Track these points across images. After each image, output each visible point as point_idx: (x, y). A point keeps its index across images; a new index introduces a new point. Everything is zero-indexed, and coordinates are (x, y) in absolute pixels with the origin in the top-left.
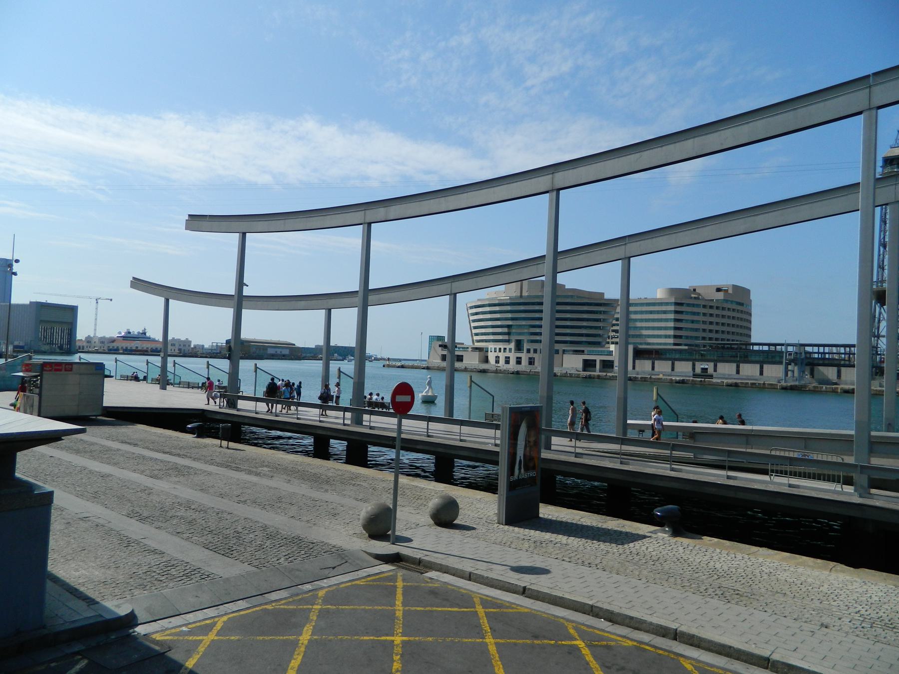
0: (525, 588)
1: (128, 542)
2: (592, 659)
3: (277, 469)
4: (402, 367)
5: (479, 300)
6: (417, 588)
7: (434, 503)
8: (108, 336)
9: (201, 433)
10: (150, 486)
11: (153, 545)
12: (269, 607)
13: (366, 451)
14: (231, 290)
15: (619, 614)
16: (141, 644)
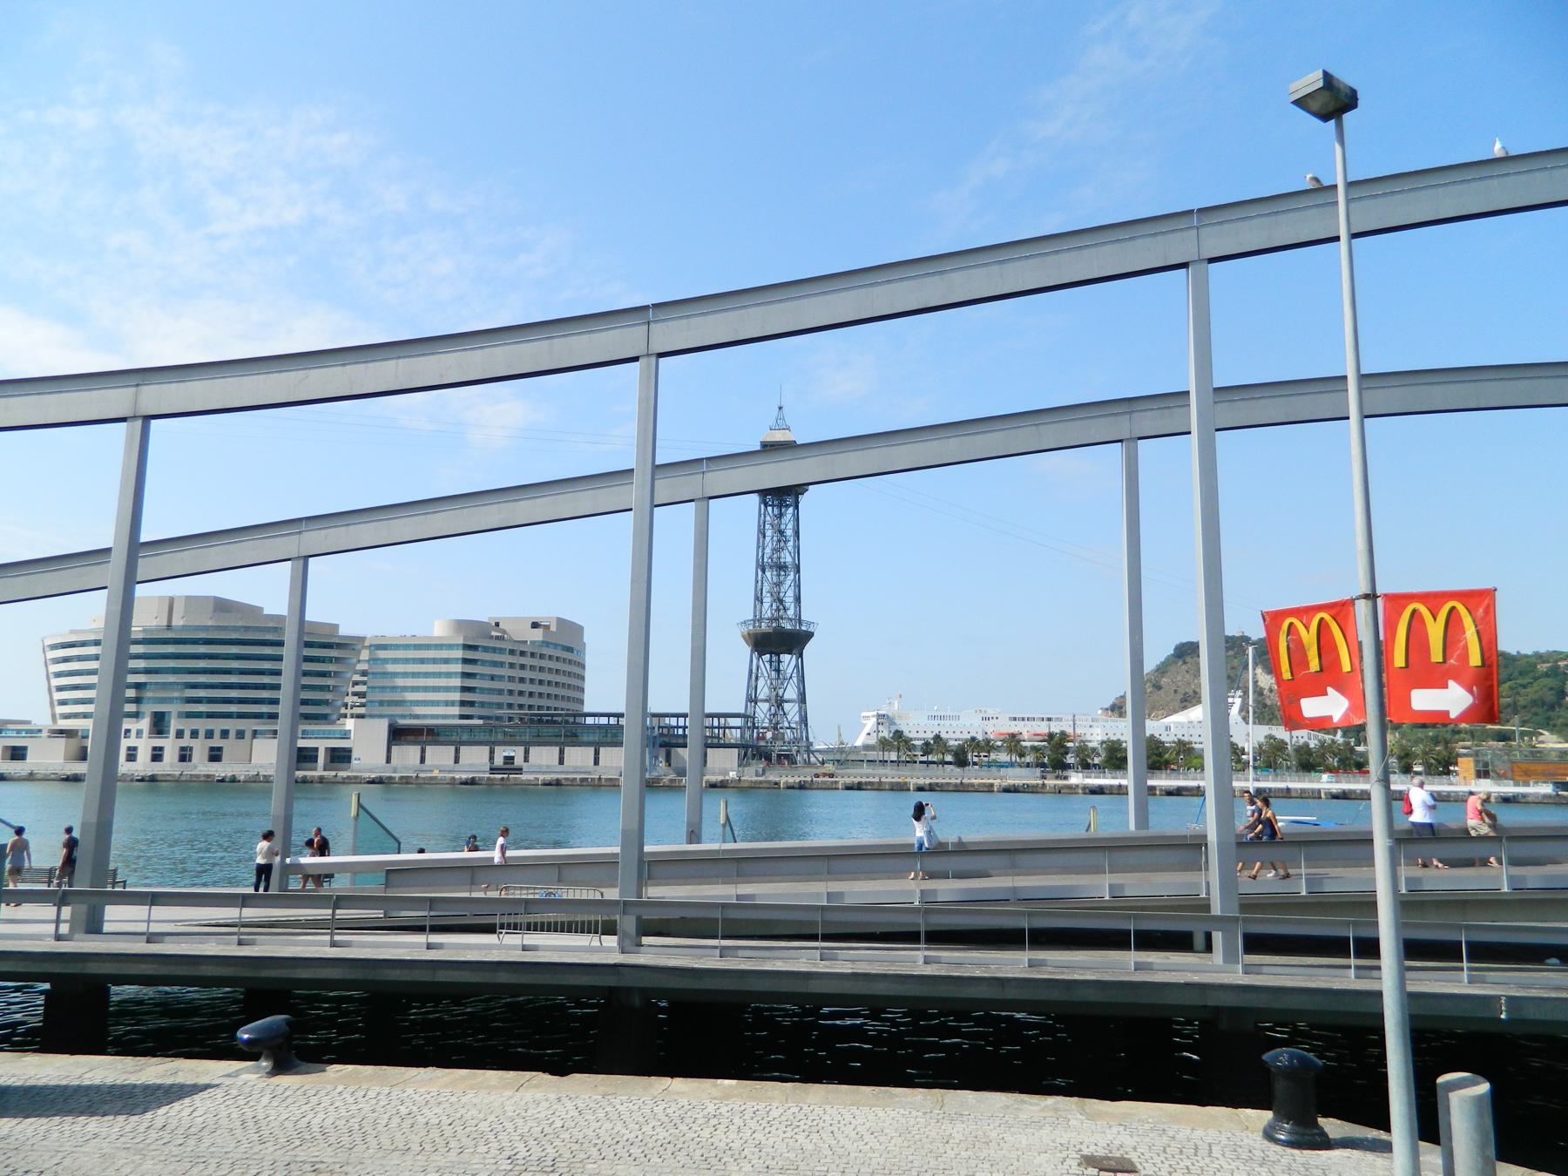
5: (73, 632)
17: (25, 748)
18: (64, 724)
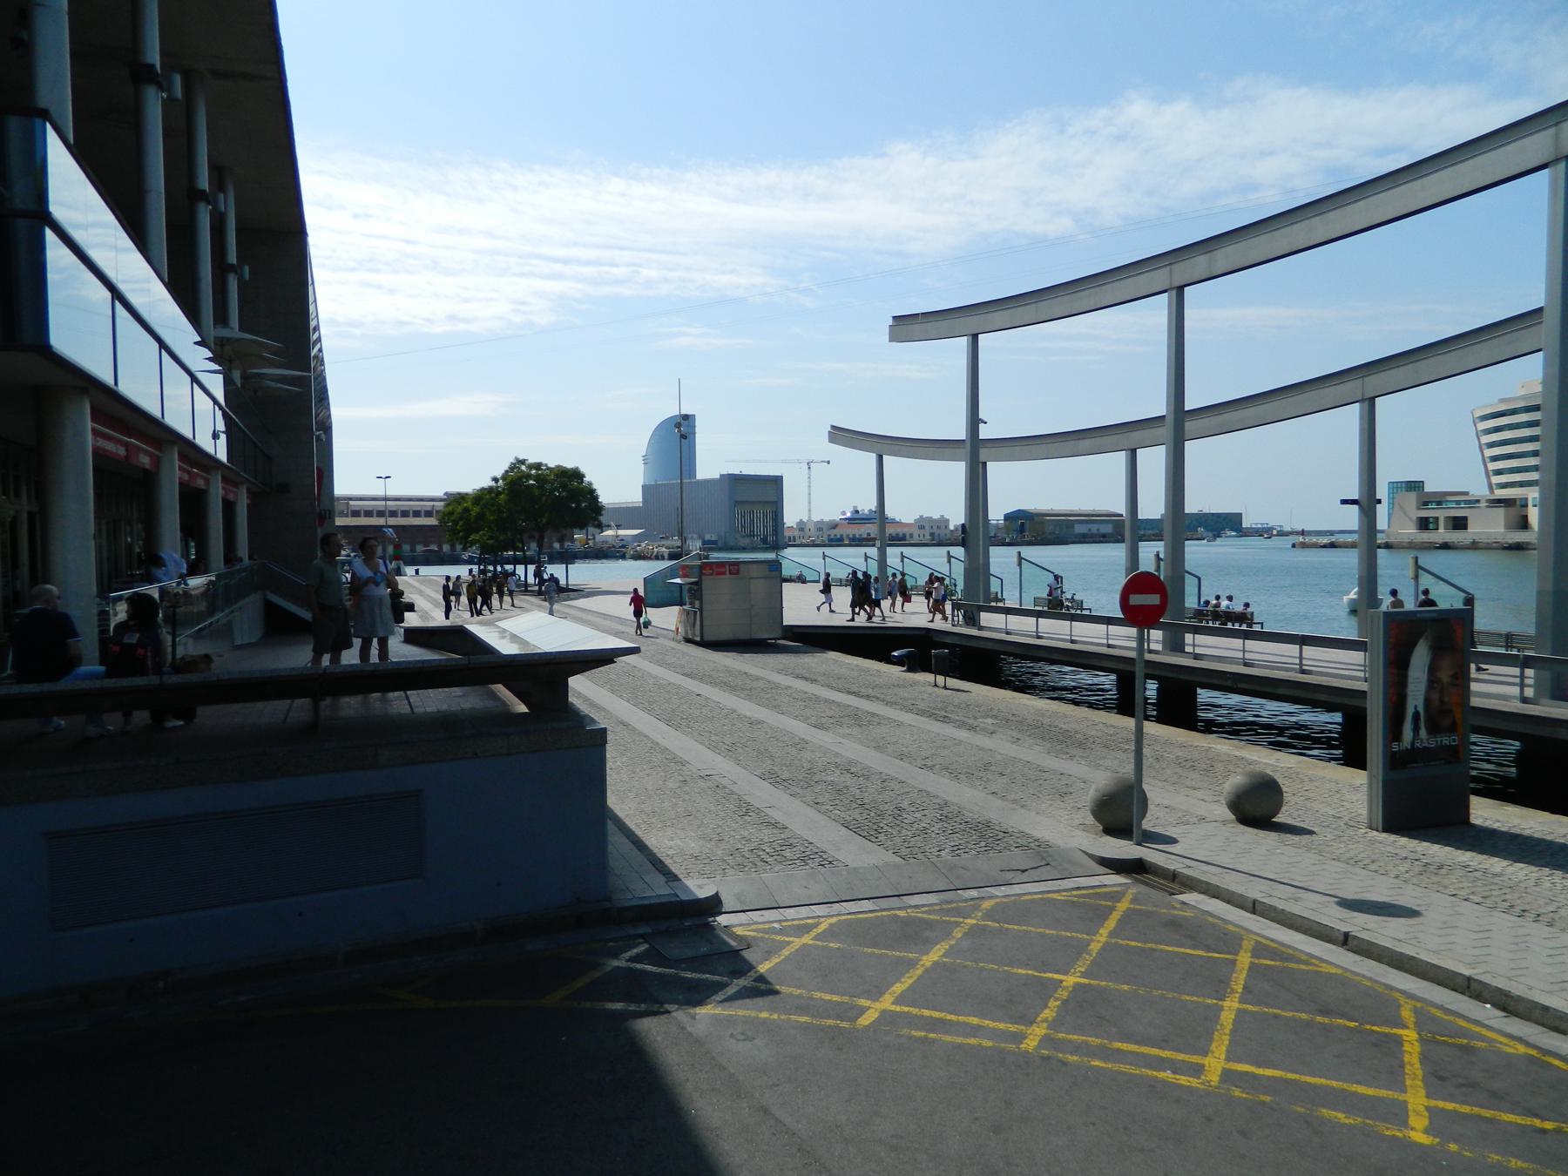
0: (1346, 935)
1: (745, 810)
2: (1416, 1061)
3: (1008, 721)
4: (1332, 545)
5: (1502, 401)
6: (1148, 914)
7: (1236, 780)
8: (826, 519)
9: (916, 663)
10: (808, 738)
11: (776, 815)
12: (901, 913)
13: (1195, 695)
14: (961, 434)
15: (1520, 999)
16: (718, 937)
17: (1465, 518)
18: (1501, 493)
